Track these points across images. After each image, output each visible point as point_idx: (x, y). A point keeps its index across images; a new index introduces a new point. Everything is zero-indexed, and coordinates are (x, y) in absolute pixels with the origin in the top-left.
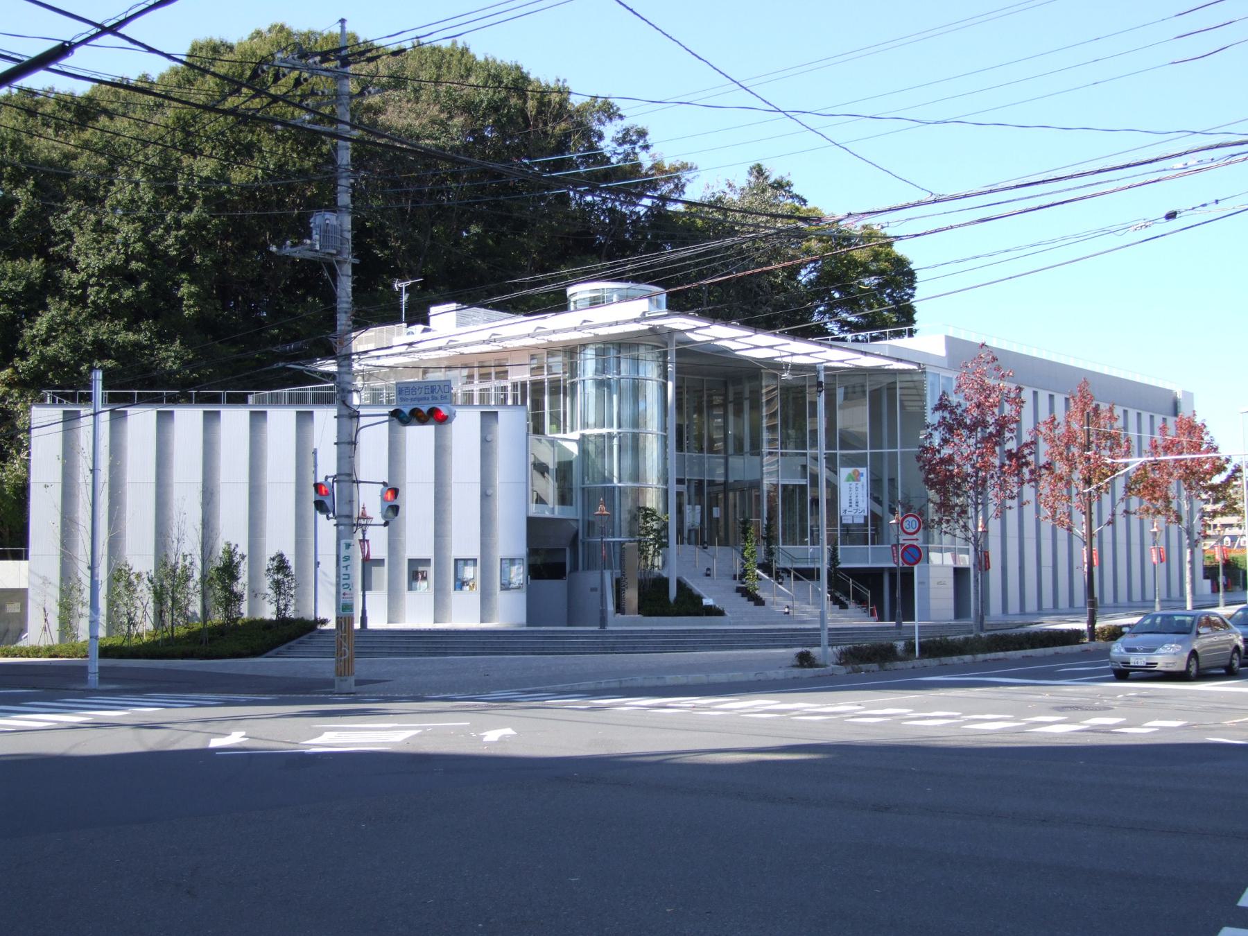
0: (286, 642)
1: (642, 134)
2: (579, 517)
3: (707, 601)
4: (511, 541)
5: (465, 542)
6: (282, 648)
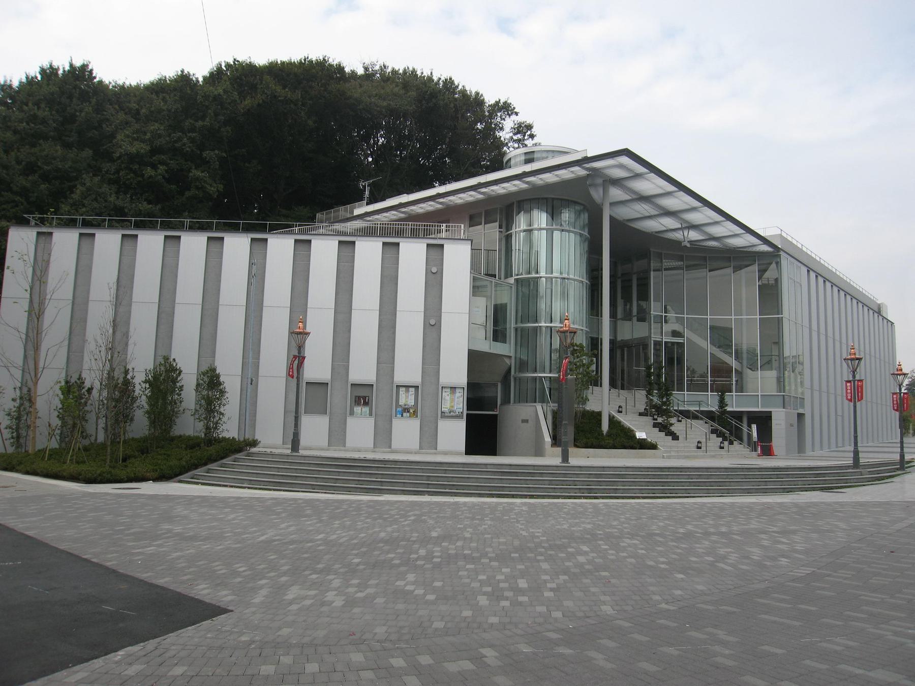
0: (205, 464)
1: (529, 127)
2: (512, 354)
3: (641, 435)
4: (455, 371)
5: (409, 368)
6: (199, 472)
